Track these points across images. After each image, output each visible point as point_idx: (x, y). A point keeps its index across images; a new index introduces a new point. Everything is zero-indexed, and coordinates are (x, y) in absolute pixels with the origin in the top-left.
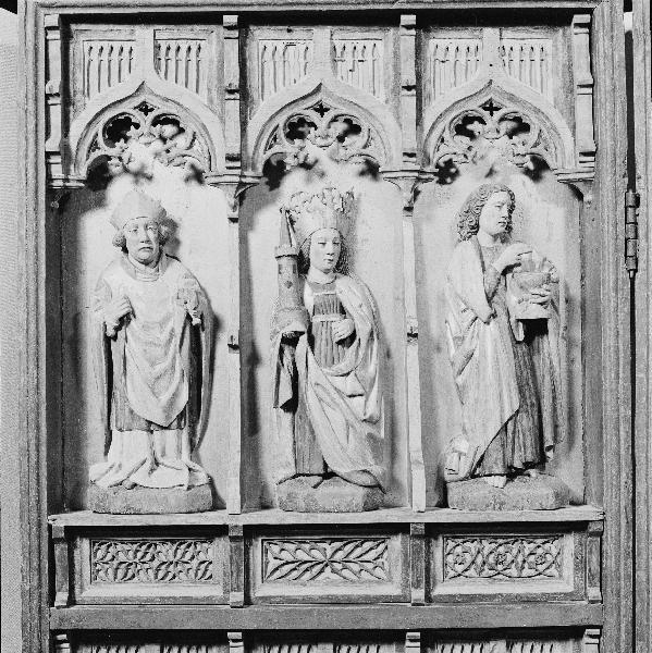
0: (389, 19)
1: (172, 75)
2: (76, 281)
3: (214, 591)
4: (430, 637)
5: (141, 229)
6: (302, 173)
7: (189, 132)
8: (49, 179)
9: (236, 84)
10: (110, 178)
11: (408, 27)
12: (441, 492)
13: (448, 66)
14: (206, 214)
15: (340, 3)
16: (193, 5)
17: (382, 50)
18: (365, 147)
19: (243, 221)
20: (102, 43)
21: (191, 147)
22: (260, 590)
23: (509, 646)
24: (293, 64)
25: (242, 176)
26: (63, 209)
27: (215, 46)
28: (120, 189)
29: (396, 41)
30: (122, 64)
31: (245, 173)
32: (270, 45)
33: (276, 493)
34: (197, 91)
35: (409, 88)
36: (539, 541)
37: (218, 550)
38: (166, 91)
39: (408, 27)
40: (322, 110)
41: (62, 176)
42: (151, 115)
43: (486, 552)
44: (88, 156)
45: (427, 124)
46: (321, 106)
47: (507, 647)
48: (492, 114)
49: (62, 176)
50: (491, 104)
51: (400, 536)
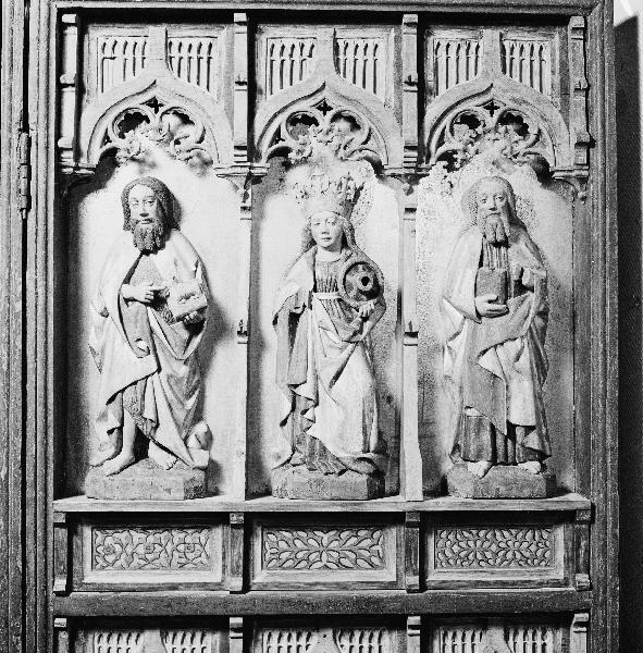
0: (223, 18)
1: (184, 73)
2: (77, 262)
3: (389, 575)
4: (255, 624)
5: (323, 223)
6: (133, 166)
7: (532, 131)
8: (59, 167)
9: (244, 77)
10: (117, 165)
11: (240, 23)
12: (257, 482)
13: (119, 63)
14: (210, 204)
15: (361, 4)
16: (455, 5)
17: (383, 51)
18: (200, 142)
19: (253, 211)
20: (202, 40)
21: (202, 140)
22: (434, 577)
23: (164, 636)
24: (306, 60)
25: (251, 168)
26: (72, 189)
27: (230, 41)
28: (125, 174)
29: (398, 39)
30: (124, 64)
31: (255, 165)
32: (131, 41)
33: (277, 479)
34: (375, 92)
35: (410, 83)
36: (362, 533)
37: (392, 537)
38: (341, 91)
39: (240, 23)
40: (325, 108)
41: (73, 164)
42: (497, 113)
43: (176, 541)
44: (271, 145)
45: (429, 120)
46: (325, 104)
47: (506, 638)
48: (325, 114)
49: (73, 164)
50: (492, 104)
51: (221, 527)
